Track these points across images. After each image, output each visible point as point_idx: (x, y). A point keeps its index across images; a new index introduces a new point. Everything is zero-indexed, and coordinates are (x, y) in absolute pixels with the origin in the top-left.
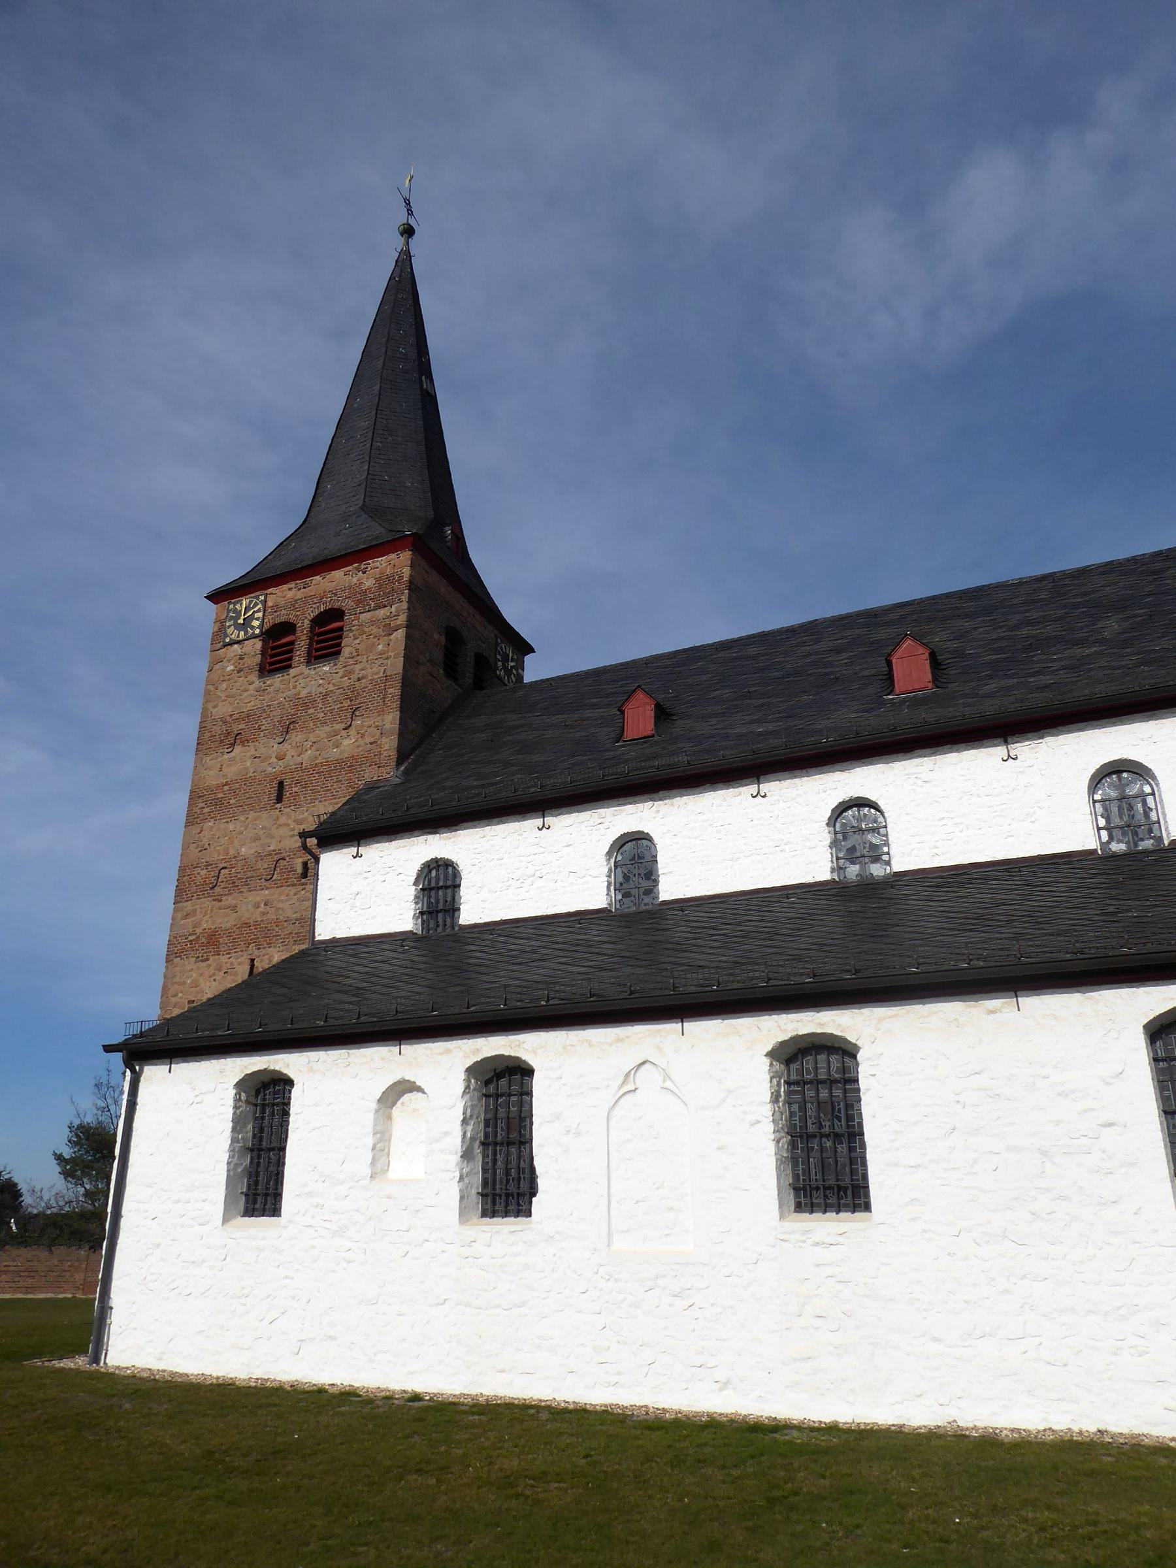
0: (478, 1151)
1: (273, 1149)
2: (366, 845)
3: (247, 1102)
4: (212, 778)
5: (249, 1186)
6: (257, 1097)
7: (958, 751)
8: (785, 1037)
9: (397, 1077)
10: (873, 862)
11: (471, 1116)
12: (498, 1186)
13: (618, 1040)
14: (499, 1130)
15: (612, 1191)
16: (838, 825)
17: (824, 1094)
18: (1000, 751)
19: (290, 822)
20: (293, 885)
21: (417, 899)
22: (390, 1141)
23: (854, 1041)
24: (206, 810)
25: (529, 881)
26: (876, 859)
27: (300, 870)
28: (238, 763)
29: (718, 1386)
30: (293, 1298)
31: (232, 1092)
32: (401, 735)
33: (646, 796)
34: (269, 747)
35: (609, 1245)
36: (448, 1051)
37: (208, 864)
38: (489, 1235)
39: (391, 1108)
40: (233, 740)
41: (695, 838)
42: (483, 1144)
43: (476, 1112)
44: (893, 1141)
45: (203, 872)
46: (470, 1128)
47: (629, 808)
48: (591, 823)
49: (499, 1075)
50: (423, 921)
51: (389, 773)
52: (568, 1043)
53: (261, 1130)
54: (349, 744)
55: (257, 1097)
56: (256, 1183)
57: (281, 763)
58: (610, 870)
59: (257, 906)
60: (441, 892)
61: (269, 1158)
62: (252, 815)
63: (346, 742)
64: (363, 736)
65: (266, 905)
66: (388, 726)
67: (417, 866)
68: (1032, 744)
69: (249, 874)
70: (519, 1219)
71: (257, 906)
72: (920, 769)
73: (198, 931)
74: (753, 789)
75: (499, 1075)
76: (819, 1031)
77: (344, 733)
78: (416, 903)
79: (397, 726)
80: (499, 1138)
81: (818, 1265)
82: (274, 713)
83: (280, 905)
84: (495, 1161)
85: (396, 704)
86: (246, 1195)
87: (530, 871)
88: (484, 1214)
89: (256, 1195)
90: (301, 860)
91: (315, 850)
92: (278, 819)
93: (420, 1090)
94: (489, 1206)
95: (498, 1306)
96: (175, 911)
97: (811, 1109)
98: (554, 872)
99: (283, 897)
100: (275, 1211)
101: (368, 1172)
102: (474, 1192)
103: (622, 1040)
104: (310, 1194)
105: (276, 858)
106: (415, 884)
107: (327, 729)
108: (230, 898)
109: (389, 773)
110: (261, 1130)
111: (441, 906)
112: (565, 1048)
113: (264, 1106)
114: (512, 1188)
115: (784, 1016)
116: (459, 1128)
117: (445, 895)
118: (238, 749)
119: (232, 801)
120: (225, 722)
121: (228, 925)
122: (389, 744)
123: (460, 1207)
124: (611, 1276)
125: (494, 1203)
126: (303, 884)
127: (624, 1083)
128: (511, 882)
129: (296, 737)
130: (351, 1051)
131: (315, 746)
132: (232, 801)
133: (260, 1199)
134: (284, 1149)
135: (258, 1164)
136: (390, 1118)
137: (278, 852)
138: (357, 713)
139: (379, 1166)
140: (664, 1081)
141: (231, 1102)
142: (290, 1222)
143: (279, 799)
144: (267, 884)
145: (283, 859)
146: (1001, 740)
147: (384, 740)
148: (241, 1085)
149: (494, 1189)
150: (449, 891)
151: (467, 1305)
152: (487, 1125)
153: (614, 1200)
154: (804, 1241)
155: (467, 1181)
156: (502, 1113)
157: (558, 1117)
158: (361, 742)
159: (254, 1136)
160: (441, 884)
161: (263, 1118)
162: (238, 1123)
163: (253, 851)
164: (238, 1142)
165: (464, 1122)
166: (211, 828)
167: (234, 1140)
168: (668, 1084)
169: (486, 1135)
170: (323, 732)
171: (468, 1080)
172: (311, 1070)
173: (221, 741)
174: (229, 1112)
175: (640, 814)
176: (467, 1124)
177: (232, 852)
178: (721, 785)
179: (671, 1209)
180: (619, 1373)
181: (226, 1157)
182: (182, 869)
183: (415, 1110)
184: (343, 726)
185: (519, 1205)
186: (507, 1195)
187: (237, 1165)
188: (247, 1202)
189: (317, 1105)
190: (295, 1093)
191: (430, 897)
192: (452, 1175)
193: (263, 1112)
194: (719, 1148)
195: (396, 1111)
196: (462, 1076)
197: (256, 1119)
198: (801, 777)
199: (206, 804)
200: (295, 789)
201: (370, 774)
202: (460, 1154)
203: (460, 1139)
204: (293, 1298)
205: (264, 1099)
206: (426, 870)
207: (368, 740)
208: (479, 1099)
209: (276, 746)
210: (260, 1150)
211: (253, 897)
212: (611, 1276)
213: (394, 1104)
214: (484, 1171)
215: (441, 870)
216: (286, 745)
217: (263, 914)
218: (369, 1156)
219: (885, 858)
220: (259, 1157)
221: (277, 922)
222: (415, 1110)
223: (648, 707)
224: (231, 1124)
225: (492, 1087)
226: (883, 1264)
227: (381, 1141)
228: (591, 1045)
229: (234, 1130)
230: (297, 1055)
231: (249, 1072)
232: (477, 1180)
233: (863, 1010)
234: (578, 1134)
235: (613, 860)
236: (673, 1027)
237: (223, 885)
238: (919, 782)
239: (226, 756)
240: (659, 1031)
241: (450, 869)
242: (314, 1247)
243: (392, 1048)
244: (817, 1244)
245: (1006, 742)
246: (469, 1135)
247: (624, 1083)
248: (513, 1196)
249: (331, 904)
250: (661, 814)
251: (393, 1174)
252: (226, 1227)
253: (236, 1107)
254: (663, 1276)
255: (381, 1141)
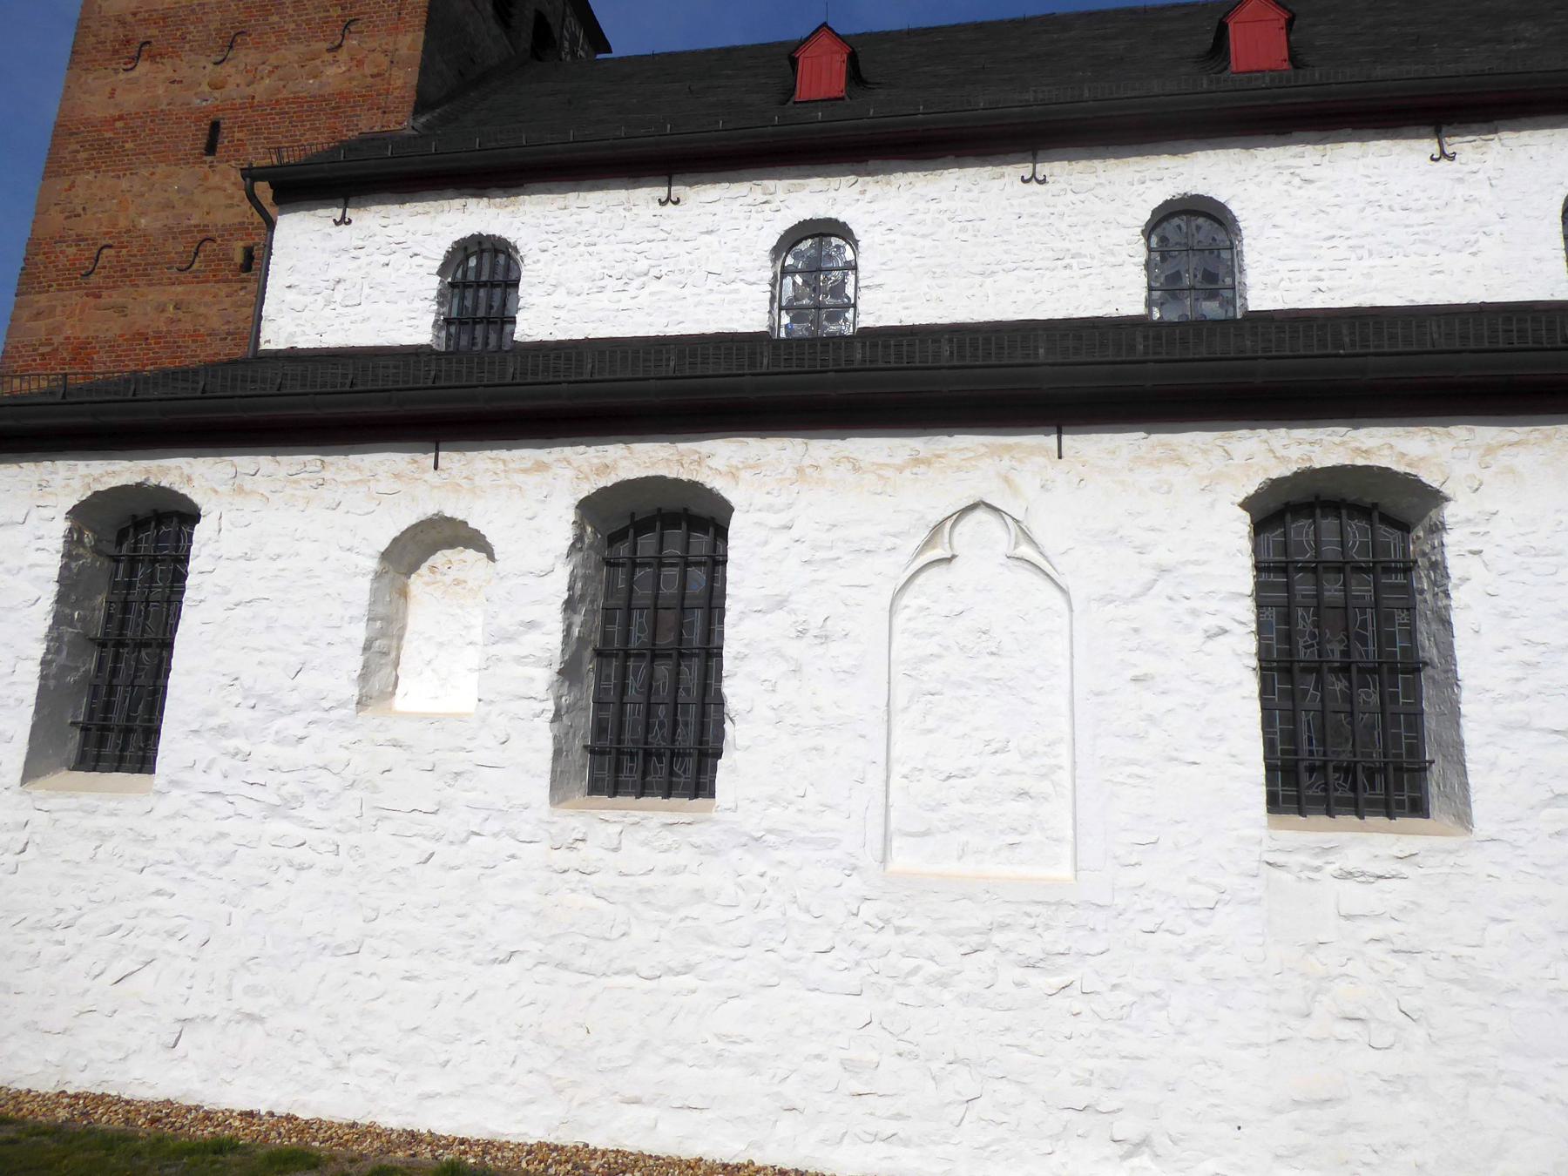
0: (589, 666)
1: (147, 645)
2: (358, 206)
3: (96, 550)
4: (96, 106)
5: (91, 712)
6: (119, 543)
7: (1362, 140)
8: (1286, 470)
9: (427, 509)
10: (1206, 299)
11: (582, 597)
12: (627, 736)
13: (917, 461)
14: (634, 629)
15: (895, 753)
16: (1154, 240)
17: (1332, 591)
18: (1429, 146)
19: (227, 185)
20: (226, 281)
21: (442, 298)
22: (401, 638)
23: (1435, 485)
24: (83, 155)
25: (637, 283)
26: (1212, 295)
27: (239, 258)
28: (144, 87)
29: (1119, 1150)
30: (171, 934)
31: (62, 526)
32: (424, 71)
33: (846, 166)
34: (198, 69)
35: (884, 861)
36: (541, 467)
37: (80, 238)
38: (618, 828)
39: (408, 574)
40: (135, 50)
41: (924, 236)
42: (599, 653)
43: (591, 591)
44: (1518, 680)
45: (72, 251)
46: (578, 619)
47: (816, 183)
48: (749, 200)
49: (641, 526)
50: (449, 335)
51: (401, 121)
52: (807, 461)
53: (126, 607)
54: (334, 74)
55: (119, 543)
56: (108, 708)
57: (217, 94)
58: (775, 276)
59: (162, 309)
60: (482, 293)
61: (138, 660)
62: (162, 169)
63: (331, 71)
64: (360, 63)
65: (176, 307)
66: (404, 52)
67: (446, 244)
68: (1478, 140)
69: (152, 259)
70: (619, 799)
71: (162, 309)
72: (1297, 162)
73: (57, 340)
74: (1025, 169)
75: (641, 526)
76: (1360, 462)
77: (328, 57)
78: (440, 304)
79: (419, 53)
80: (634, 644)
81: (1348, 917)
82: (211, 17)
83: (202, 310)
84: (623, 689)
85: (420, 20)
86: (85, 729)
87: (643, 264)
88: (595, 788)
89: (104, 729)
90: (241, 244)
91: (271, 210)
92: (206, 178)
93: (475, 541)
94: (606, 775)
95: (629, 971)
96: (18, 306)
97: (1304, 621)
98: (682, 271)
99: (208, 298)
100: (144, 762)
101: (354, 692)
102: (578, 744)
103: (927, 462)
104: (222, 730)
105: (199, 237)
106: (440, 273)
107: (301, 48)
108: (115, 294)
109: (401, 121)
110: (126, 607)
111: (481, 313)
112: (800, 470)
113: (133, 562)
114: (658, 740)
115: (1283, 431)
116: (560, 617)
117: (490, 298)
118: (143, 67)
119: (127, 146)
120: (123, 23)
121: (110, 335)
122: (405, 79)
123: (553, 771)
124: (888, 921)
125: (618, 769)
126: (243, 281)
127: (928, 543)
128: (607, 281)
129: (245, 56)
130: (328, 459)
131: (279, 72)
132: (127, 146)
133: (112, 737)
134: (169, 645)
135: (114, 672)
136: (404, 593)
137: (203, 228)
138: (352, 28)
139: (376, 683)
140: (1017, 544)
141: (58, 544)
142: (174, 783)
143: (211, 148)
144: (182, 276)
145: (213, 240)
146: (1430, 129)
147: (395, 71)
148: (81, 514)
149: (620, 741)
150: (498, 291)
151: (561, 965)
152: (608, 618)
153: (898, 770)
154: (1318, 869)
155: (566, 720)
156: (643, 593)
157: (781, 603)
158: (355, 72)
159: (109, 617)
160: (484, 278)
161: (130, 586)
162: (70, 586)
163: (158, 225)
164: (71, 624)
165: (570, 605)
166: (89, 184)
167: (59, 619)
168: (1025, 550)
169: (606, 637)
170: (291, 53)
171: (579, 525)
172: (240, 490)
173: (116, 52)
174: (52, 564)
175: (832, 194)
176: (575, 611)
177: (123, 223)
178: (971, 159)
179: (1023, 794)
180: (899, 1116)
181: (39, 650)
182: (34, 244)
183: (457, 582)
184: (326, 45)
185: (672, 773)
186: (648, 754)
187: (64, 670)
188: (85, 742)
189: (246, 557)
190: (201, 532)
191: (463, 298)
192: (538, 707)
193: (132, 572)
194: (1135, 680)
195: (418, 583)
196: (571, 516)
197: (115, 585)
198: (1103, 157)
199: (79, 146)
200: (238, 135)
201: (368, 123)
202: (557, 667)
203: (559, 637)
204: (171, 934)
205: (135, 549)
206: (460, 256)
207: (368, 70)
208: (598, 569)
209: (210, 66)
210: (120, 644)
211: (154, 295)
212: (888, 921)
213: (414, 568)
214: (599, 703)
215: (486, 257)
216: (227, 68)
217: (172, 321)
218: (356, 663)
219: (1228, 294)
220: (117, 658)
221: (195, 336)
222: (457, 582)
223: (838, 57)
224: (55, 588)
225: (623, 550)
226: (1494, 920)
227: (383, 634)
228: (856, 469)
229: (61, 599)
230: (210, 460)
231: (102, 488)
232: (586, 720)
233: (1452, 429)
234: (824, 638)
235: (779, 264)
236: (1040, 443)
237: (104, 273)
238: (1296, 181)
239: (122, 76)
240: (1009, 448)
241: (502, 258)
242: (223, 835)
243: (419, 456)
244: (1348, 875)
245: (1438, 134)
246: (576, 631)
247: (928, 543)
248: (660, 756)
249: (290, 296)
250: (868, 196)
251: (400, 703)
252: (29, 787)
253: (67, 555)
254: (1004, 926)
255: (383, 634)
